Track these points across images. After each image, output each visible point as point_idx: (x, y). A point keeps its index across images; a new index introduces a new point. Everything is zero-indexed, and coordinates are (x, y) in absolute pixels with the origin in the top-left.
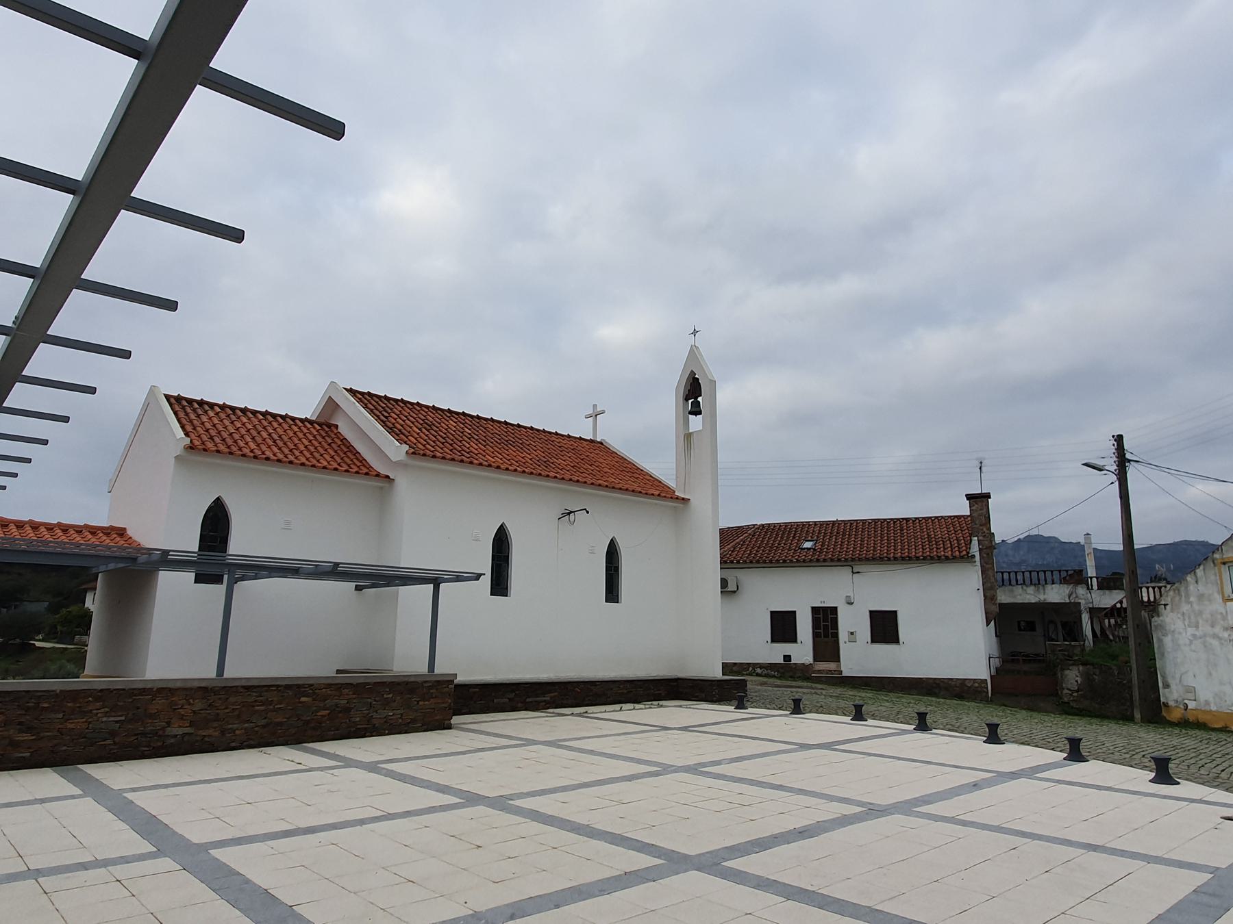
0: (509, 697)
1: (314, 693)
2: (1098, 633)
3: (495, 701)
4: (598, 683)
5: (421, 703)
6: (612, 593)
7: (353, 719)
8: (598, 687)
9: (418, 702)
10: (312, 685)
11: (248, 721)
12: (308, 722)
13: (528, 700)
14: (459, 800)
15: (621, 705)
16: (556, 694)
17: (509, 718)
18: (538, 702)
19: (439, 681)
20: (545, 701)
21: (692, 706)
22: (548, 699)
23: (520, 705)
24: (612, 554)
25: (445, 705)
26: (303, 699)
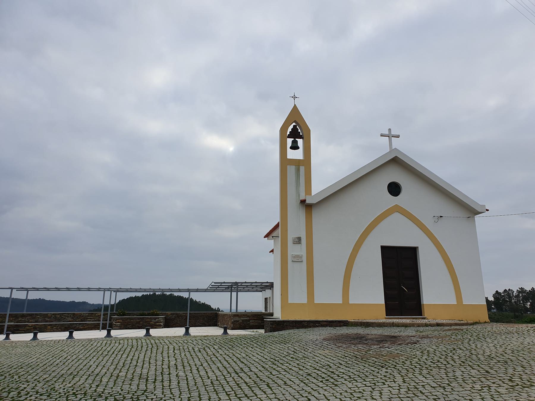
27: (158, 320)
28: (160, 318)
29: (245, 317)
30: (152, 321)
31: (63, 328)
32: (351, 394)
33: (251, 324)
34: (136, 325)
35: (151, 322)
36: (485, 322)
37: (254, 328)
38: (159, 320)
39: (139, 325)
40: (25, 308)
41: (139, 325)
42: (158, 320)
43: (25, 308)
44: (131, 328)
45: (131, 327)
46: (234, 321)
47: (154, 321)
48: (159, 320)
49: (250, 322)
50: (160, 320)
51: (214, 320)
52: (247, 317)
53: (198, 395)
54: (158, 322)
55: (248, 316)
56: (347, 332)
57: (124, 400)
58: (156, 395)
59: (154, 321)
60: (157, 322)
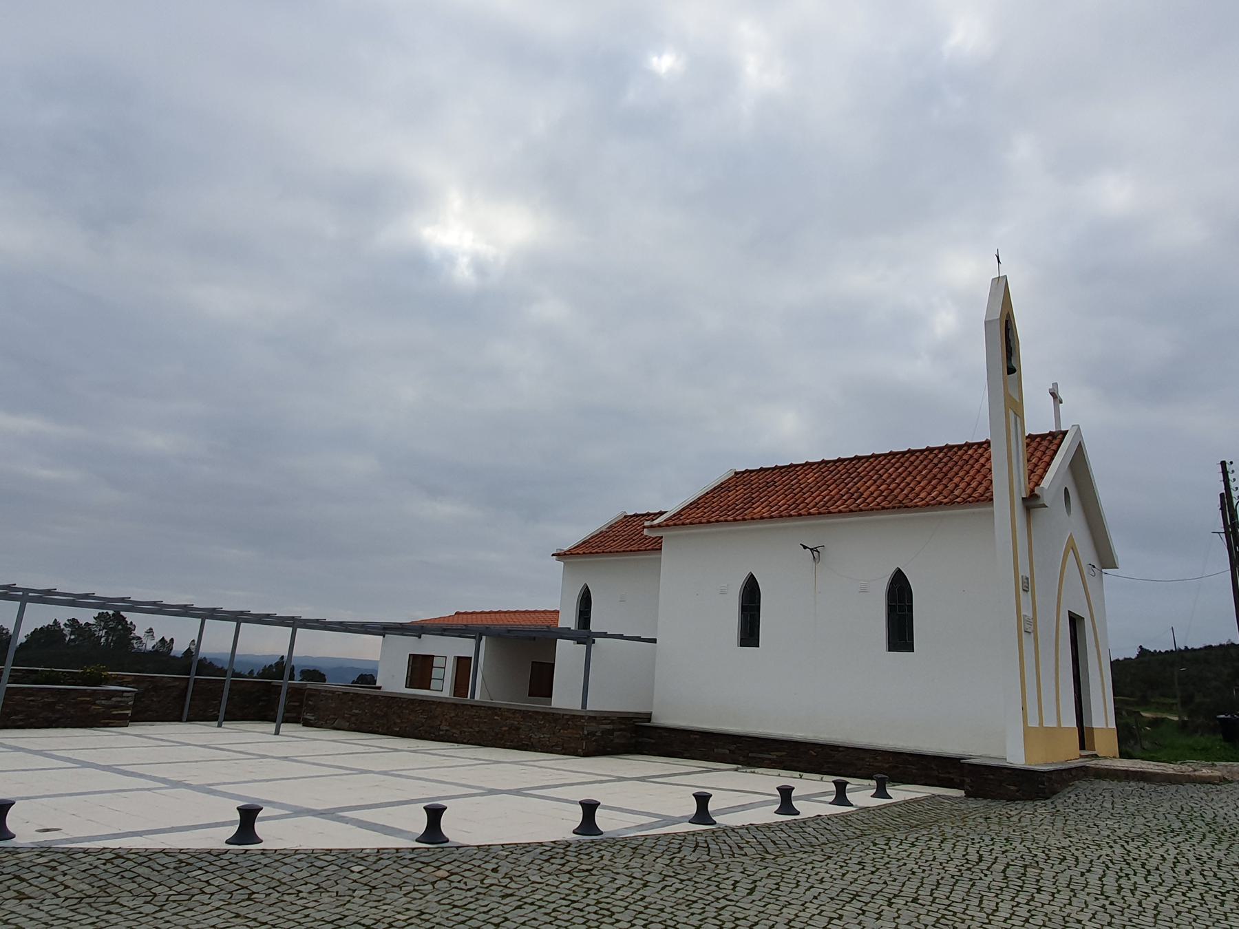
0: (730, 748)
1: (502, 714)
2: (18, 850)
3: (715, 750)
4: (841, 749)
5: (562, 731)
6: (750, 634)
7: (521, 736)
8: (841, 754)
9: (560, 730)
10: (500, 709)
11: (471, 728)
12: (497, 734)
13: (750, 755)
14: (287, 812)
15: (822, 776)
16: (785, 753)
17: (769, 773)
18: (763, 759)
19: (574, 715)
20: (770, 759)
21: (536, 763)
22: (775, 757)
23: (741, 758)
24: (751, 595)
25: (578, 736)
26: (496, 718)
27: (119, 699)
28: (125, 694)
29: (606, 724)
30: (97, 702)
31: (1074, 773)
32: (1150, 872)
33: (617, 741)
34: (41, 716)
35: (94, 707)
36: (1114, 757)
37: (54, 725)
38: (123, 699)
39: (50, 715)
40: (226, 693)
41: (50, 715)
42: (119, 699)
43: (226, 693)
44: (20, 723)
45: (21, 720)
46: (588, 734)
47: (103, 702)
48: (123, 699)
49: (615, 735)
50: (126, 699)
51: (260, 704)
52: (609, 724)
53: (977, 861)
54: (116, 708)
55: (612, 722)
56: (1184, 767)
57: (830, 926)
58: (915, 863)
59: (103, 702)
60: (116, 707)
